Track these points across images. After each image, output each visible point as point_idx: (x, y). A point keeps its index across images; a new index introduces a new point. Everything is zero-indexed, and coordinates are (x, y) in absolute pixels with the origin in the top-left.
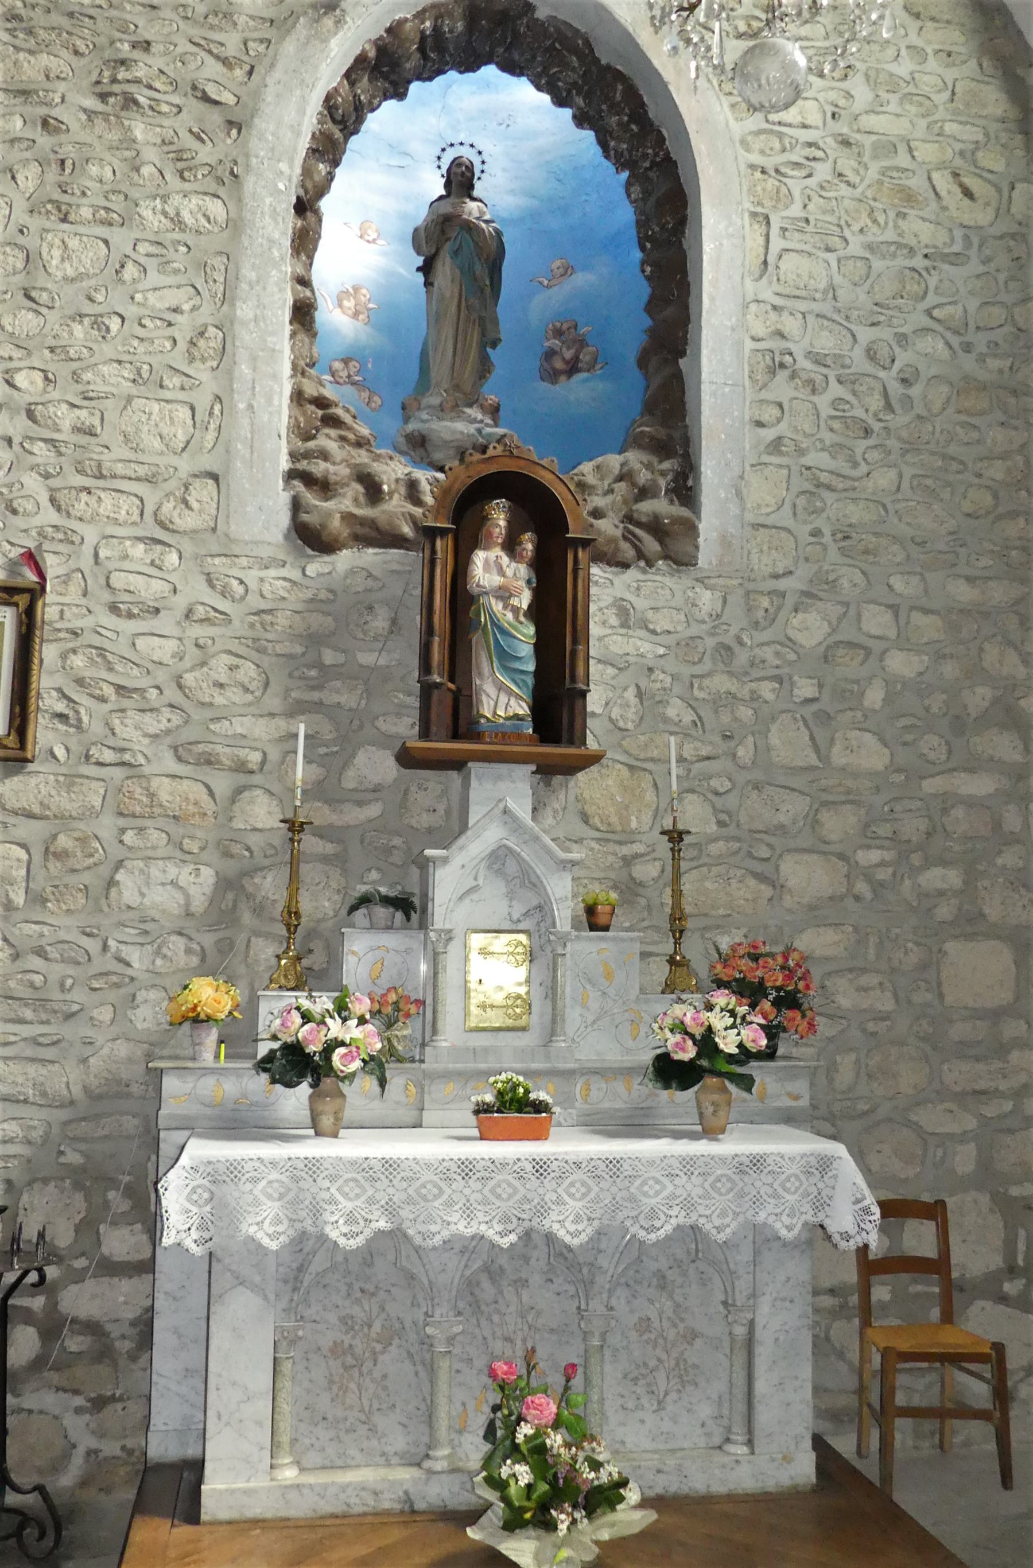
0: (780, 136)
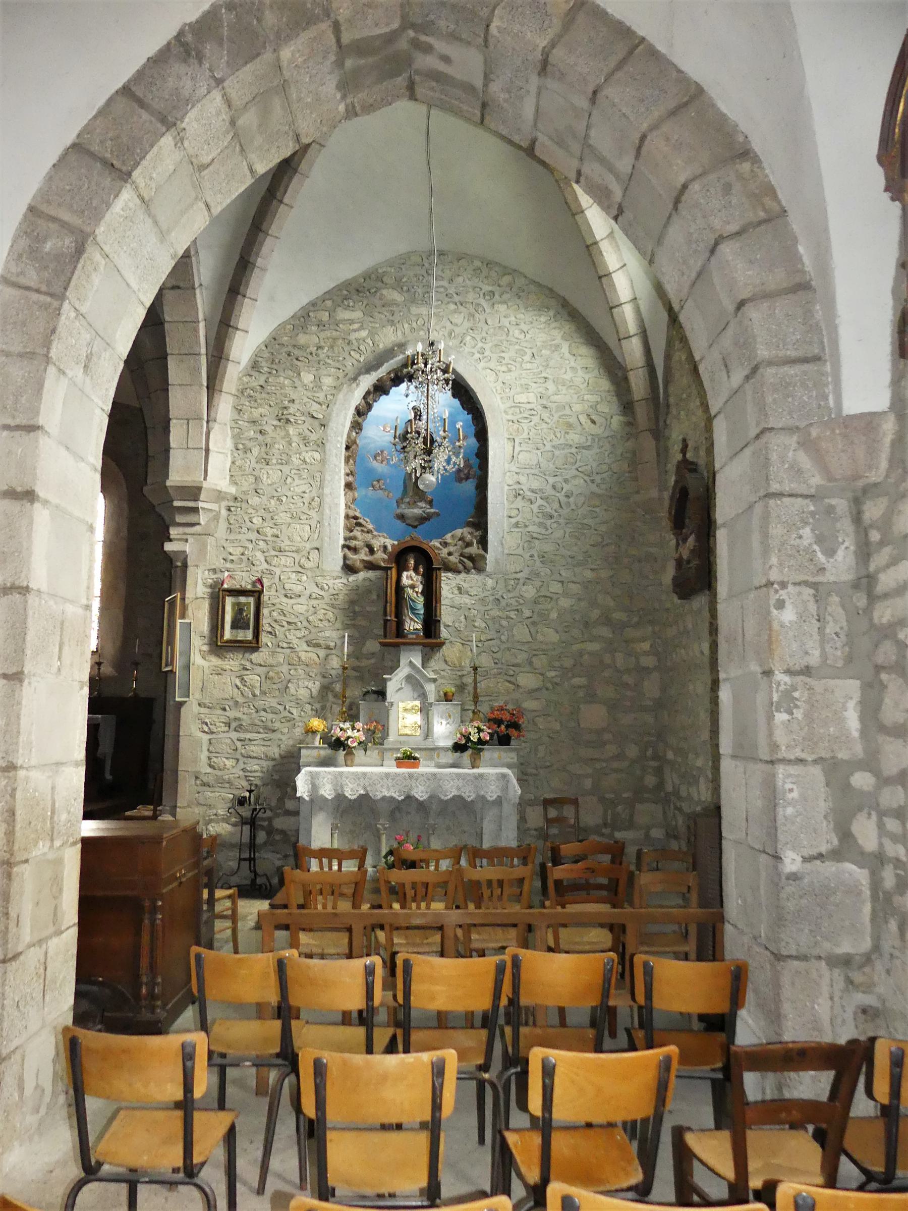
0: (519, 407)
